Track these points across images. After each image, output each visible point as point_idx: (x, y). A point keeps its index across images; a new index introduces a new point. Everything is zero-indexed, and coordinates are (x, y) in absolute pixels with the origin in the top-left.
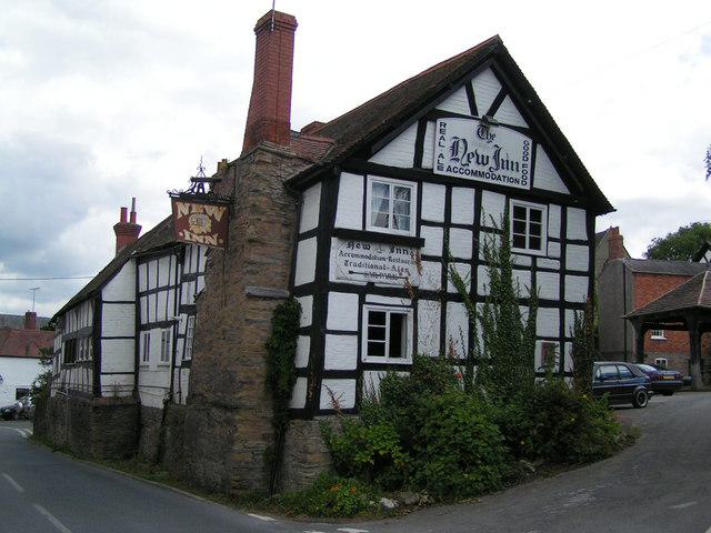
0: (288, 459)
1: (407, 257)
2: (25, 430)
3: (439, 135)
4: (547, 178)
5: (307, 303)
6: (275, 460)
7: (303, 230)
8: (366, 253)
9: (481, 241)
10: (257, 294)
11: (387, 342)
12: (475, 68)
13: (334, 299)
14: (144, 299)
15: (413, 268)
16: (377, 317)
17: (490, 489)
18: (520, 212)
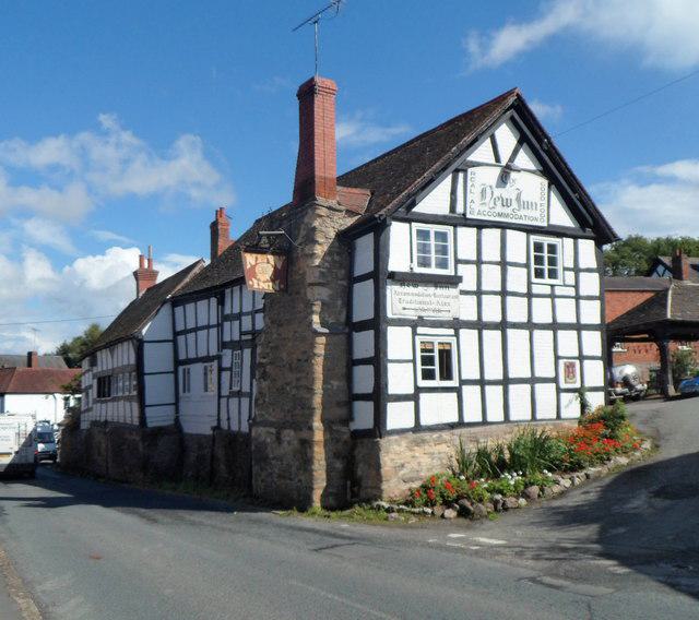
4: (561, 217)
7: (358, 272)
14: (181, 339)
18: (539, 247)
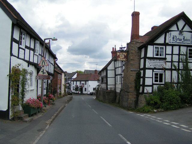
0: (139, 102)
1: (163, 62)
2: (94, 97)
3: (170, 36)
5: (142, 72)
6: (136, 102)
8: (154, 61)
9: (180, 57)
10: (133, 70)
11: (159, 79)
12: (178, 19)
13: (147, 71)
14: (116, 69)
15: (164, 64)
16: (156, 74)
17: (176, 109)
